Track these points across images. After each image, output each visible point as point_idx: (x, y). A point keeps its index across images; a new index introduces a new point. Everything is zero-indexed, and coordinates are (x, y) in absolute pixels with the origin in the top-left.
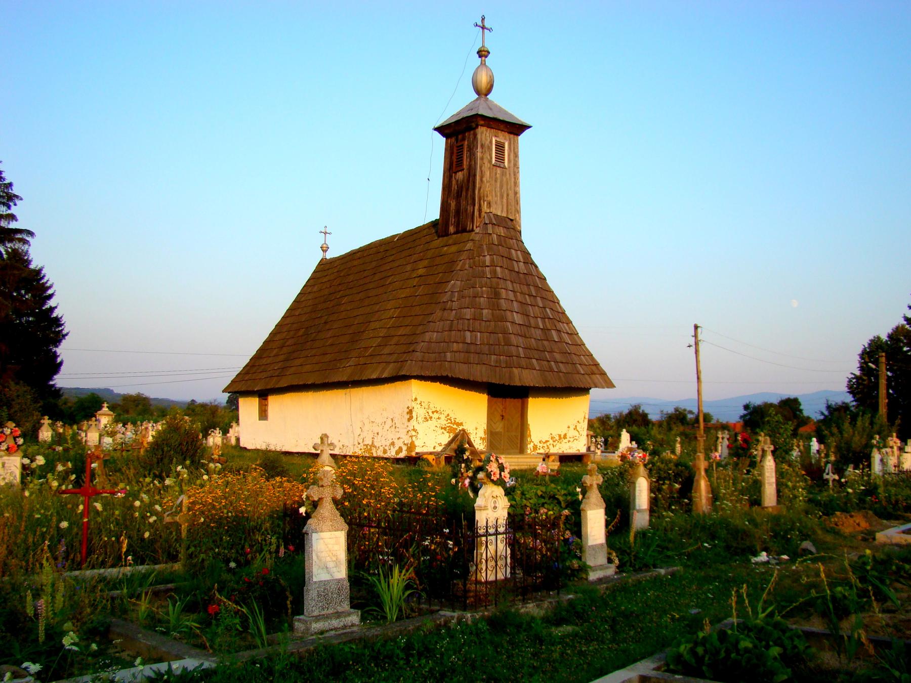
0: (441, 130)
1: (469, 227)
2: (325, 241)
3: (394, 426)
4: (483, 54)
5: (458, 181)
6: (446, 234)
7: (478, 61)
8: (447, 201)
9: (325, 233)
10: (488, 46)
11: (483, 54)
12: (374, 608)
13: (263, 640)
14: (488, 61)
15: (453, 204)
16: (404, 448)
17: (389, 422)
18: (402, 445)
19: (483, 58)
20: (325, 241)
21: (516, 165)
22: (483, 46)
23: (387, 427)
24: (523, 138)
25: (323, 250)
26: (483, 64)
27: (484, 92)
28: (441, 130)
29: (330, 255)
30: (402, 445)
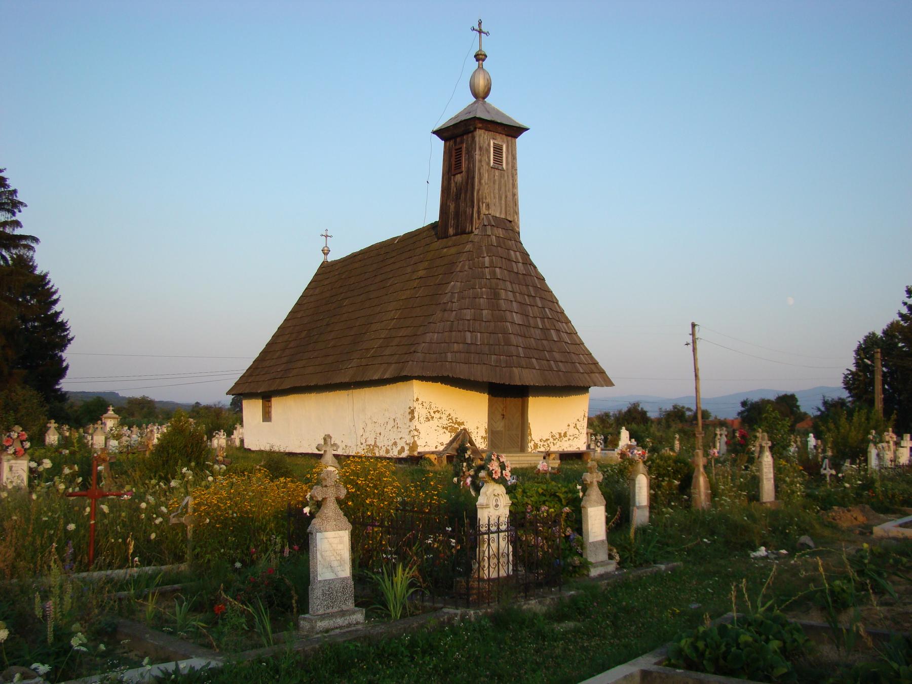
0: (439, 133)
1: (468, 229)
2: (480, 45)
3: (396, 426)
4: (480, 57)
5: (456, 183)
6: (446, 236)
7: (476, 64)
8: (446, 204)
9: (326, 236)
10: (485, 50)
11: (480, 57)
12: (378, 606)
13: (269, 639)
14: (486, 64)
15: (452, 206)
16: (407, 448)
17: (391, 423)
18: (404, 445)
19: (481, 62)
20: (480, 45)
21: (514, 167)
22: (326, 246)
23: (389, 427)
24: (521, 141)
25: (324, 253)
26: (480, 67)
27: (481, 95)
28: (439, 133)
29: (331, 258)
30: (404, 445)
